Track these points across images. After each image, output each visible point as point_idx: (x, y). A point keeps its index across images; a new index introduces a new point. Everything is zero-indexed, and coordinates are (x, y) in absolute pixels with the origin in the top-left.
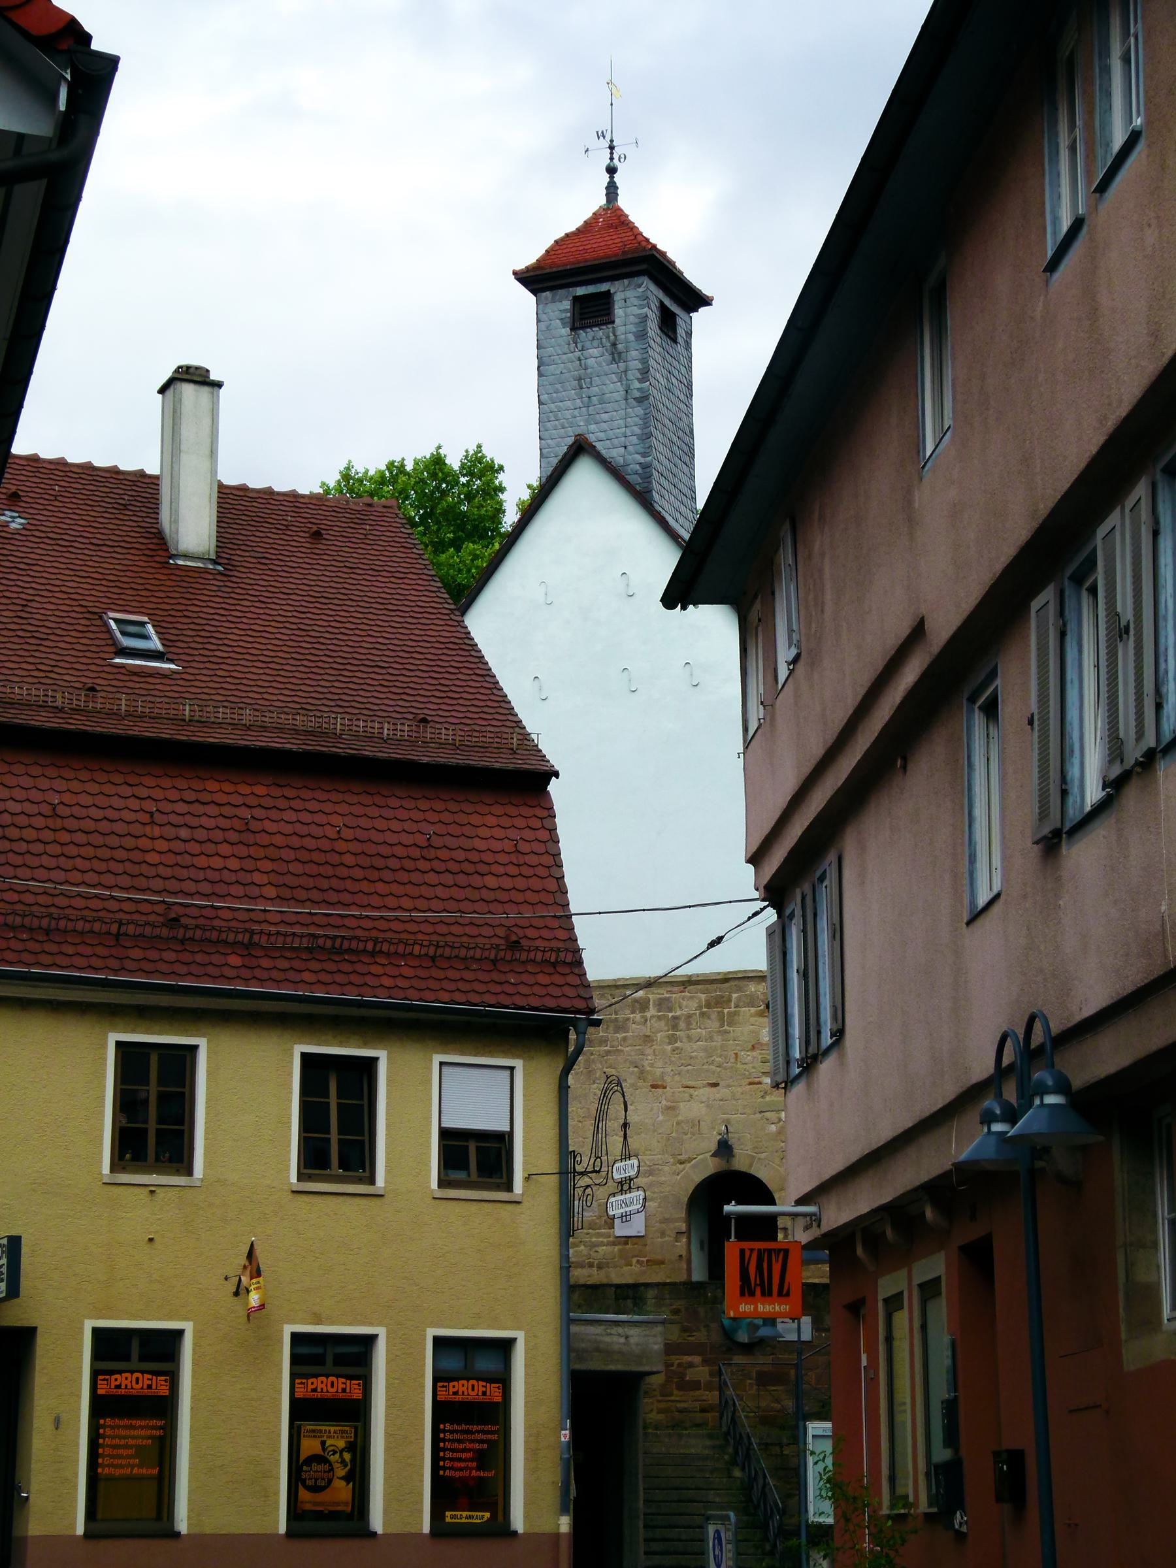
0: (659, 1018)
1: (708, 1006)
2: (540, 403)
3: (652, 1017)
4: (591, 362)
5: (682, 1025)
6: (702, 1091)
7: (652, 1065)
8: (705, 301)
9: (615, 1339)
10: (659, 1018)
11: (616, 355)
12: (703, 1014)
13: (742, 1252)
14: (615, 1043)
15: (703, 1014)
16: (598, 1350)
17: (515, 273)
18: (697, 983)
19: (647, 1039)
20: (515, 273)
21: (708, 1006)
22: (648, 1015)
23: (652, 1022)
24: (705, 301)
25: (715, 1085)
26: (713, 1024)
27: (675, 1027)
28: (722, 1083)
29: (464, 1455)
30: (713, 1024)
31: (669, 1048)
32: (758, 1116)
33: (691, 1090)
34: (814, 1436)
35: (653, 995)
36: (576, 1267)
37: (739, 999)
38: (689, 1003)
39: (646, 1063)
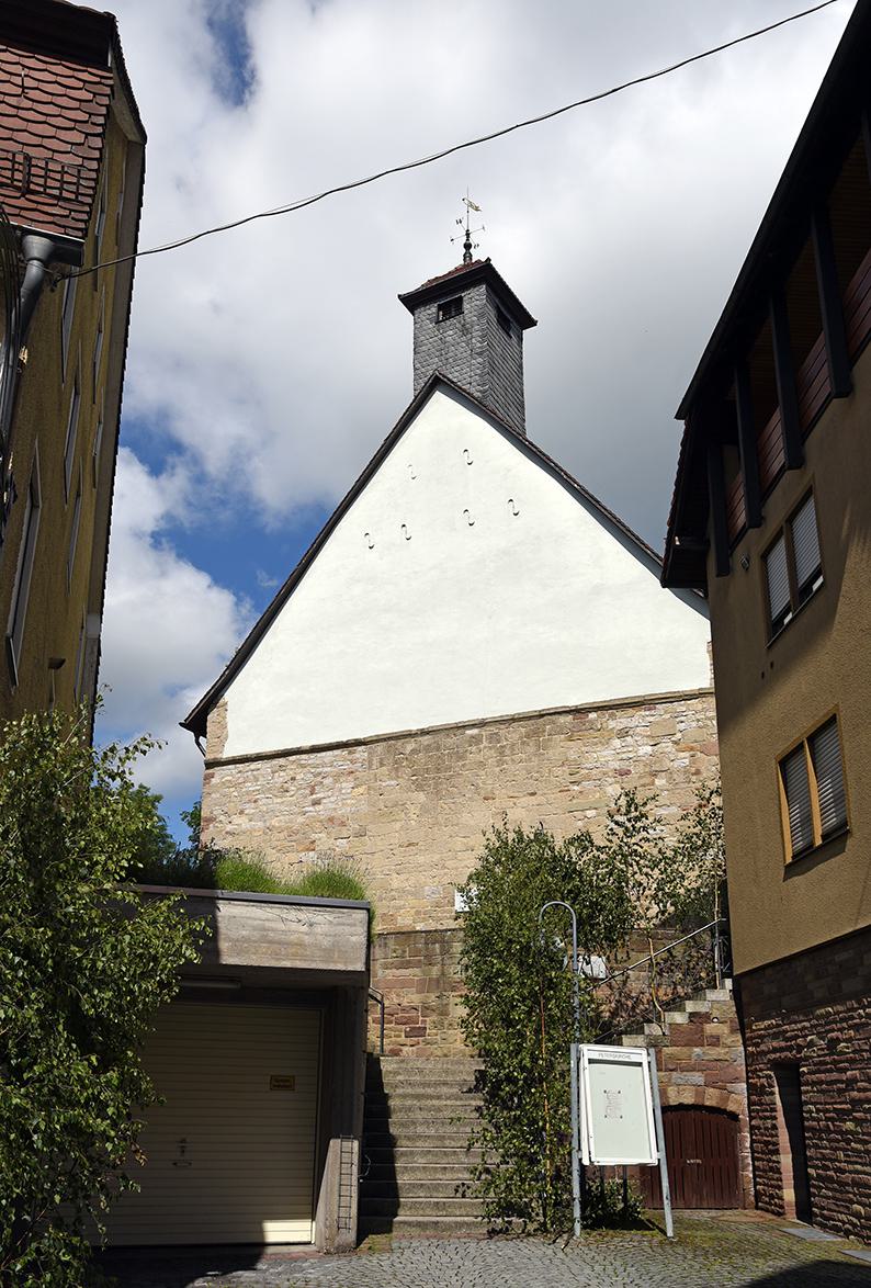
0: (490, 748)
1: (528, 736)
2: (415, 369)
3: (485, 747)
4: (448, 339)
5: (508, 752)
6: (524, 799)
7: (484, 783)
8: (533, 323)
9: (294, 926)
10: (490, 748)
11: (465, 330)
12: (523, 743)
13: (640, 1064)
14: (457, 769)
15: (523, 743)
16: (265, 940)
17: (399, 296)
18: (520, 719)
19: (482, 764)
20: (399, 296)
21: (528, 736)
22: (482, 746)
23: (486, 753)
24: (533, 323)
25: (533, 794)
26: (531, 749)
27: (502, 754)
28: (539, 792)
29: (445, 1090)
30: (531, 749)
31: (498, 769)
32: (567, 815)
33: (515, 800)
34: (591, 1061)
35: (485, 732)
36: (667, 1098)
37: (552, 729)
38: (515, 733)
39: (480, 782)
